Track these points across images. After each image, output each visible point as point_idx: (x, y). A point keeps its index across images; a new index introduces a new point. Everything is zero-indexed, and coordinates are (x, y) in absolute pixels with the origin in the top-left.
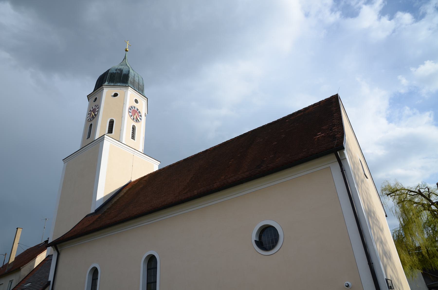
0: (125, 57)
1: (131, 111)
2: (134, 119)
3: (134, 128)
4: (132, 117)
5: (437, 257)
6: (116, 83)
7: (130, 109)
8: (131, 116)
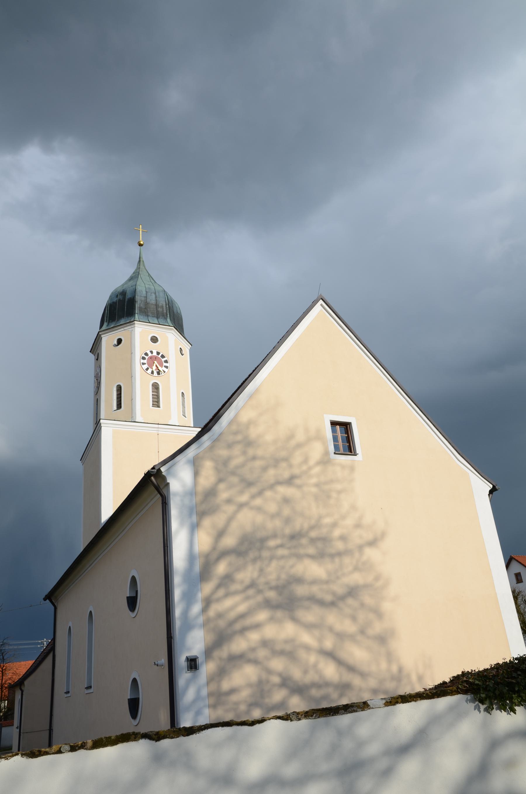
0: (140, 258)
1: (145, 361)
2: (152, 372)
3: (156, 387)
4: (150, 371)
5: (481, 772)
6: (118, 320)
7: (144, 358)
8: (147, 369)
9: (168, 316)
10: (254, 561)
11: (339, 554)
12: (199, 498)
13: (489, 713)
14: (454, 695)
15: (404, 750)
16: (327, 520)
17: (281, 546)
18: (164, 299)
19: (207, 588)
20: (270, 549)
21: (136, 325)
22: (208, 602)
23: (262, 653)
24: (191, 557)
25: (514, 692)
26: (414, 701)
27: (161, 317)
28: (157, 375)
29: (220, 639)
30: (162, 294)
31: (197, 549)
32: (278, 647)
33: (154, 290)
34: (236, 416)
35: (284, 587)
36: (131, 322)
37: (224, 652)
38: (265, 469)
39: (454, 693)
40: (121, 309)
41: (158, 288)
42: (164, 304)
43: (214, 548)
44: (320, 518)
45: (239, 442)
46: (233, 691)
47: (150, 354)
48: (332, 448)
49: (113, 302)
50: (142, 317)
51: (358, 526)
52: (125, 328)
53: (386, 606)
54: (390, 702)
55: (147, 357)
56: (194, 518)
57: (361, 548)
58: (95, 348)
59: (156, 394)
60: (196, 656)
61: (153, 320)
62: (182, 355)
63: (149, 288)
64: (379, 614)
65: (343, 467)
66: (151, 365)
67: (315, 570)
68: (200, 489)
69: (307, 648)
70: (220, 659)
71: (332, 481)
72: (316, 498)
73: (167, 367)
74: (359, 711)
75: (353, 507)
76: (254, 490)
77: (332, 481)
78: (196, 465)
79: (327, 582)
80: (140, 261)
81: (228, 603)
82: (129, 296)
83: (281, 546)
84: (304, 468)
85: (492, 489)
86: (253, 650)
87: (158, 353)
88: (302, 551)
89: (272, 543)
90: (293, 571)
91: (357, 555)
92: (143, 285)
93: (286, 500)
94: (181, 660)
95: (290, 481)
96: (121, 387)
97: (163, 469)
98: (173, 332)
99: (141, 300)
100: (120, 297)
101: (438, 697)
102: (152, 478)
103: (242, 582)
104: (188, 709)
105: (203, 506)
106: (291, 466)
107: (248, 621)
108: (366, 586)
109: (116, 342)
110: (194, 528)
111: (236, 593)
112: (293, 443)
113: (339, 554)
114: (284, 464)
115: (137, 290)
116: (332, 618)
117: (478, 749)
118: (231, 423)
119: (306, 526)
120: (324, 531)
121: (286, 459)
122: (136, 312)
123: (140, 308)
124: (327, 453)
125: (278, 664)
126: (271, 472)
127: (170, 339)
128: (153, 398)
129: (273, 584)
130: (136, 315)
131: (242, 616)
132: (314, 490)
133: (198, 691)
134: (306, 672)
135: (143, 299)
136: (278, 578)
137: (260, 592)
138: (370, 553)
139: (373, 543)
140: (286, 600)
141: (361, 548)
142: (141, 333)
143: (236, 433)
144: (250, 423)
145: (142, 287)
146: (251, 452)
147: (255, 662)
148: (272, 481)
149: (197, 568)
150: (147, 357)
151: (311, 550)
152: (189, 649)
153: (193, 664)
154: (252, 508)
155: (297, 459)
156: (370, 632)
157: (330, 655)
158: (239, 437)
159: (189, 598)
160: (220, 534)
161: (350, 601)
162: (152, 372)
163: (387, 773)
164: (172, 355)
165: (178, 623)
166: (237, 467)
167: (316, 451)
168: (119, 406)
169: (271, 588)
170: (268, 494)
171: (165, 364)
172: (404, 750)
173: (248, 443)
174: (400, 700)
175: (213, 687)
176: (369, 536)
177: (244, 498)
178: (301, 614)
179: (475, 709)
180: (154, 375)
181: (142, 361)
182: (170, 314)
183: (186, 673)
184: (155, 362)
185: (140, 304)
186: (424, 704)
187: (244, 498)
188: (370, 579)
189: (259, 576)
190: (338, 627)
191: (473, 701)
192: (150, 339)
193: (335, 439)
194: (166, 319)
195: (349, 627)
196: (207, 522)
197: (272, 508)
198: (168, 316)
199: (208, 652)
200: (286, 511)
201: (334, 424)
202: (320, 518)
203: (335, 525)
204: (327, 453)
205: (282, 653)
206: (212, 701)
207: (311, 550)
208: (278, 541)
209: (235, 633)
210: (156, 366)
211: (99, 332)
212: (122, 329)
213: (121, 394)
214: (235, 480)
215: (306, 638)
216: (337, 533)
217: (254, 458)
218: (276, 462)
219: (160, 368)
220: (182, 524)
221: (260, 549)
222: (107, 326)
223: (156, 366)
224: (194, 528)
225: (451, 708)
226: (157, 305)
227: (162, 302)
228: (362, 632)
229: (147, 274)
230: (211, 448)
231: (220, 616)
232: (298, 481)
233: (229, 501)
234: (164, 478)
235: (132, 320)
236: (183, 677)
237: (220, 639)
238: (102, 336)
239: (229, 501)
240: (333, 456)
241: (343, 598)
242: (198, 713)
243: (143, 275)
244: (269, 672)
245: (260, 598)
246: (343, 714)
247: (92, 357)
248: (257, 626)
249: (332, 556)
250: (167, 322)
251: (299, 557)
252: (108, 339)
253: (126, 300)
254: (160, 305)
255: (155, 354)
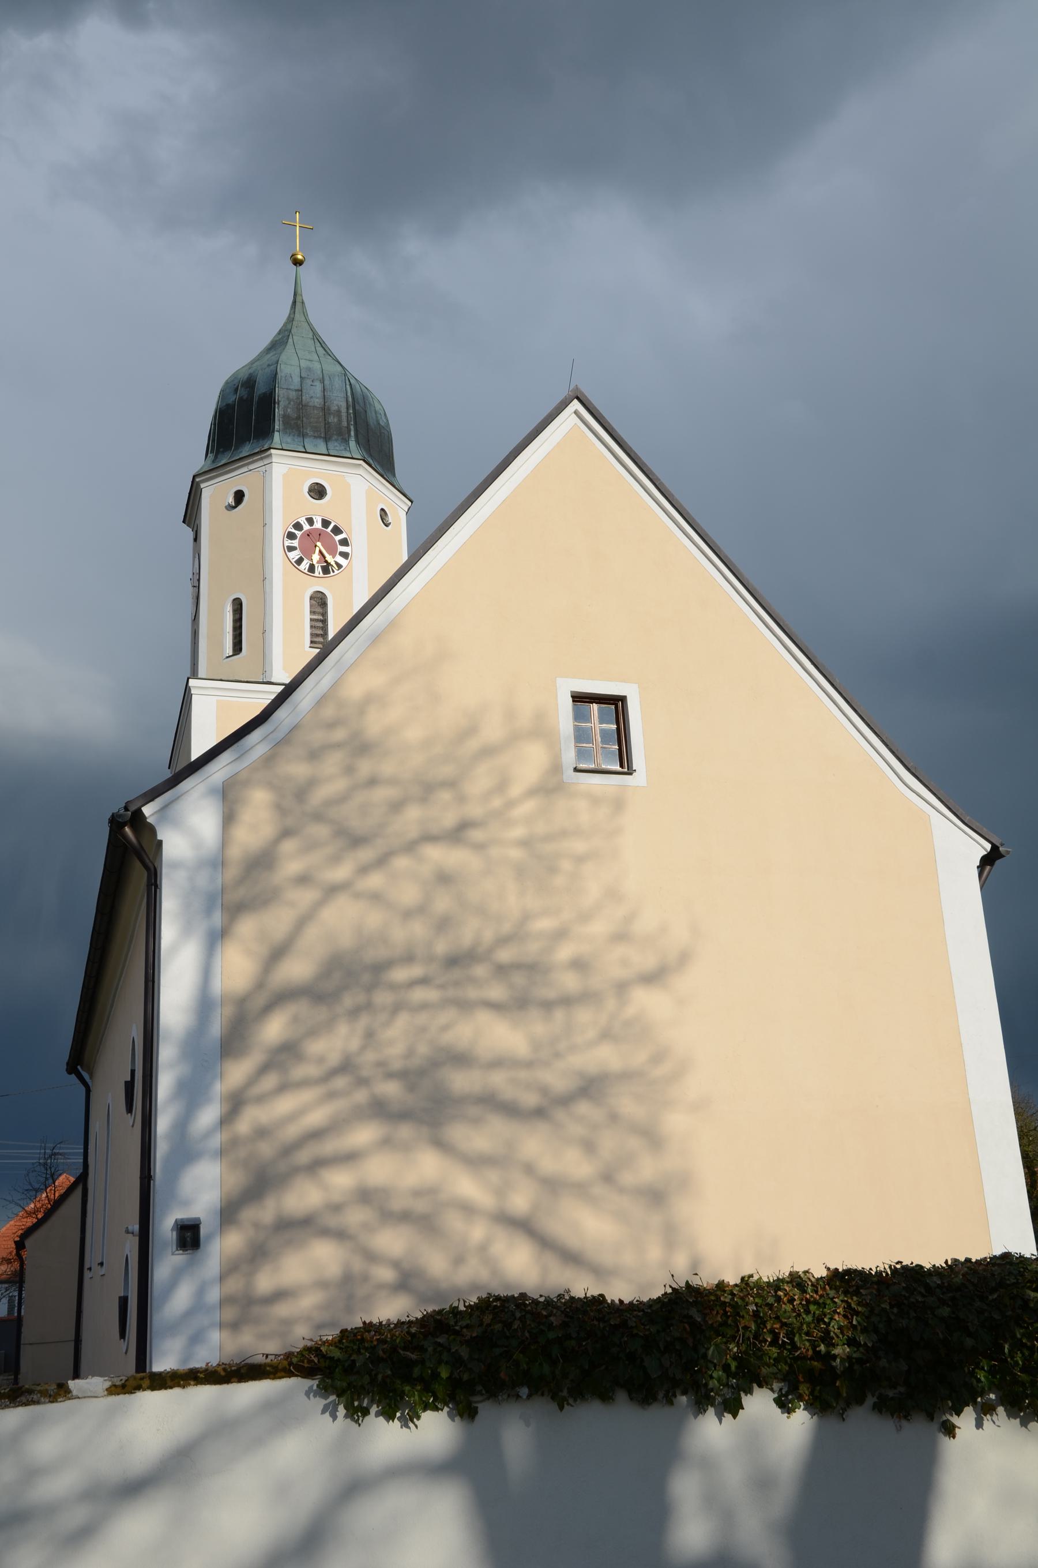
1: (295, 543)
2: (312, 569)
4: (305, 565)
7: (291, 536)
8: (300, 561)
9: (352, 433)
10: (354, 1013)
11: (567, 1001)
12: (232, 872)
13: (357, 1421)
14: (280, 1378)
15: (133, 1488)
16: (544, 924)
17: (424, 981)
18: (343, 395)
19: (237, 1073)
20: (393, 987)
21: (274, 459)
22: (235, 1104)
23: (356, 1217)
24: (204, 1004)
25: (408, 1379)
26: (179, 1386)
27: (335, 437)
28: (321, 575)
29: (260, 1183)
30: (338, 383)
31: (217, 986)
32: (397, 1205)
33: (319, 372)
34: (335, 686)
35: (422, 1072)
36: (263, 453)
37: (266, 1212)
38: (396, 807)
39: (279, 1374)
40: (245, 422)
41: (331, 368)
42: (343, 405)
43: (260, 985)
44: (526, 917)
45: (338, 746)
46: (280, 1295)
47: (306, 527)
48: (569, 756)
49: (228, 405)
50: (289, 440)
51: (621, 937)
52: (251, 467)
53: (675, 1122)
54: (123, 1386)
55: (298, 533)
56: (217, 918)
57: (622, 988)
58: (191, 515)
59: (321, 617)
60: (198, 1219)
61: (316, 446)
62: (387, 525)
63: (309, 369)
64: (652, 1138)
65: (595, 800)
66: (308, 553)
67: (501, 1035)
68: (235, 852)
69: (468, 1209)
70: (257, 1226)
71: (563, 834)
72: (520, 872)
73: (345, 555)
74: (44, 1403)
75: (613, 894)
76: (366, 854)
77: (563, 834)
78: (229, 801)
79: (529, 1064)
80: (294, 302)
81: (285, 1105)
82: (261, 388)
83: (424, 981)
84: (497, 803)
85: (989, 854)
86: (336, 1208)
87: (326, 523)
88: (472, 993)
89: (400, 974)
90: (448, 1038)
91: (611, 1004)
92: (295, 361)
93: (444, 878)
94: (165, 1225)
95: (457, 834)
96: (241, 604)
97: (148, 810)
98: (361, 471)
99: (288, 399)
100: (243, 392)
101: (239, 1381)
102: (127, 829)
103: (321, 1060)
104: (173, 1329)
105: (239, 891)
106: (461, 799)
107: (329, 1147)
108: (627, 1076)
109: (231, 500)
110: (216, 939)
111: (305, 1083)
112: (473, 744)
113: (567, 1001)
114: (445, 796)
115: (279, 376)
116: (534, 1144)
117: (309, 1495)
118: (321, 702)
119: (488, 936)
120: (532, 949)
121: (451, 784)
122: (277, 427)
123: (286, 419)
124: (556, 768)
125: (392, 1242)
126: (413, 813)
127: (356, 490)
128: (311, 627)
129: (397, 1065)
130: (276, 434)
131: (316, 1135)
132: (515, 854)
133: (200, 1292)
134: (459, 1260)
135: (293, 395)
136: (410, 1053)
137: (362, 1082)
138: (647, 1001)
139: (653, 978)
140: (426, 1101)
141: (622, 988)
142: (286, 474)
143: (332, 725)
144: (369, 700)
145: (291, 366)
146: (365, 767)
147: (340, 1235)
148: (413, 833)
149: (216, 1029)
150: (298, 533)
151: (497, 992)
152: (186, 1203)
153: (189, 1236)
154: (358, 896)
155: (480, 781)
156: (628, 1178)
157: (524, 1226)
158: (339, 735)
159: (192, 1093)
160: (277, 953)
161: (583, 1108)
162: (312, 569)
163: (82, 1536)
164: (359, 527)
165: (161, 1149)
166: (330, 803)
167: (530, 763)
168: (238, 647)
169: (390, 1075)
170: (402, 863)
171: (342, 549)
172: (133, 1488)
173: (361, 747)
174: (146, 1383)
175: (234, 1285)
176: (645, 961)
177: (341, 873)
178: (460, 1134)
179: (323, 1412)
180: (316, 574)
181: (288, 543)
182: (356, 431)
183: (173, 1254)
184: (319, 544)
185: (286, 408)
186: (204, 1394)
187: (341, 873)
188: (639, 1058)
189: (363, 1048)
190: (548, 1165)
191: (324, 1390)
192: (306, 489)
193: (581, 736)
194: (346, 441)
195: (576, 1165)
196: (247, 927)
197: (408, 894)
198: (352, 433)
199: (228, 1214)
200: (442, 903)
201: (580, 698)
202: (526, 917)
203: (561, 934)
204: (556, 768)
205: (405, 1217)
206: (230, 1313)
207: (497, 992)
208: (416, 971)
209: (296, 1171)
210: (320, 552)
211: (194, 477)
212: (245, 469)
213: (241, 619)
214: (321, 831)
215: (467, 1186)
216: (564, 953)
217: (373, 782)
218: (427, 790)
219: (329, 558)
220: (187, 930)
221: (370, 989)
222: (213, 462)
223: (320, 552)
224: (216, 939)
225: (267, 1406)
226: (325, 409)
227: (339, 401)
228: (608, 1177)
229: (311, 335)
230: (269, 760)
231: (262, 1132)
232: (477, 835)
233: (303, 880)
234: (152, 830)
235: (266, 447)
236: (166, 1264)
237: (260, 1183)
238: (202, 485)
239: (303, 880)
240: (569, 774)
241: (565, 1101)
242: (196, 1339)
243: (300, 337)
244: (371, 1256)
245: (361, 1096)
246: (7, 1407)
247: (189, 533)
248: (349, 1158)
249: (548, 1006)
250: (347, 448)
251: (465, 1006)
252: (215, 494)
253: (256, 399)
254: (334, 408)
255: (318, 525)
